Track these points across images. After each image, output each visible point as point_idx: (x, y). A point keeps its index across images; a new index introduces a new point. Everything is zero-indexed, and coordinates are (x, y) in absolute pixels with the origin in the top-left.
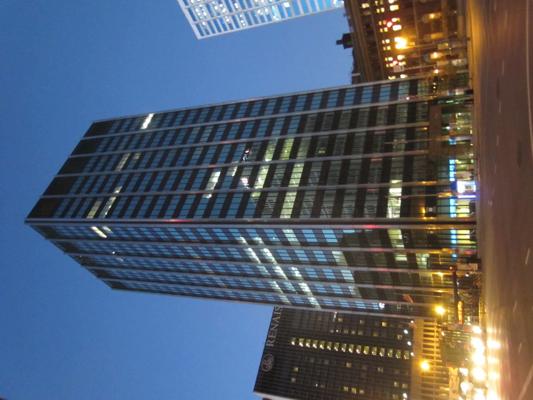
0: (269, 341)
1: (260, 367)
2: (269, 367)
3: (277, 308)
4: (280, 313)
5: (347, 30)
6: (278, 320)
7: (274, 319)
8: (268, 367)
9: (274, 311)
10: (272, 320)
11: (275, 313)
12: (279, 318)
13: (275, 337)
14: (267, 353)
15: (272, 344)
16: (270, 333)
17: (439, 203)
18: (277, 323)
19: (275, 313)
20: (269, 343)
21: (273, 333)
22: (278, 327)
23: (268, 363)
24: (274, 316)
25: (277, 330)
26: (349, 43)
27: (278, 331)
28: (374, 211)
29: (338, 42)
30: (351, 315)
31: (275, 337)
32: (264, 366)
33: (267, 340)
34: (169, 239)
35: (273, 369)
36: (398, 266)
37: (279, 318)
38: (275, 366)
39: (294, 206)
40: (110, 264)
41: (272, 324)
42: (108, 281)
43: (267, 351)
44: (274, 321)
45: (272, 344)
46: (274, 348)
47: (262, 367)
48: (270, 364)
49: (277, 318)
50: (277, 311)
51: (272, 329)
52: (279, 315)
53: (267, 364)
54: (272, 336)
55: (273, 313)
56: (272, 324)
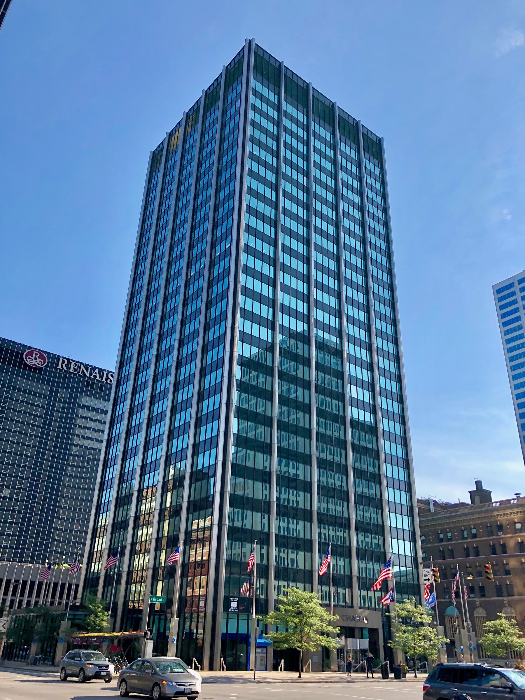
0: (66, 362)
1: (30, 348)
2: (28, 360)
3: (112, 376)
4: (104, 380)
5: (495, 498)
6: (95, 376)
7: (97, 370)
8: (29, 358)
9: (109, 372)
10: (96, 368)
11: (105, 373)
12: (98, 378)
13: (71, 370)
14: (49, 359)
15: (62, 366)
16: (78, 364)
17: (243, 616)
18: (90, 375)
19: (105, 373)
20: (63, 362)
21: (78, 368)
22: (84, 374)
23: (36, 359)
24: (101, 371)
25: (80, 374)
26: (477, 499)
27: (80, 376)
28: (238, 512)
29: (478, 484)
30: (95, 480)
31: (71, 370)
32: (31, 354)
33: (68, 360)
34: (222, 167)
35: (26, 365)
36: (152, 617)
37: (98, 378)
38: (30, 368)
39: (248, 468)
40: (186, 154)
41: (90, 368)
42: (163, 148)
43: (54, 359)
44: (94, 370)
45: (62, 366)
46: (57, 369)
47: (31, 351)
48: (34, 361)
49: (98, 375)
50: (107, 377)
51: (82, 367)
52: (102, 379)
53: (33, 358)
54: (72, 367)
55: (105, 370)
56: (90, 368)
